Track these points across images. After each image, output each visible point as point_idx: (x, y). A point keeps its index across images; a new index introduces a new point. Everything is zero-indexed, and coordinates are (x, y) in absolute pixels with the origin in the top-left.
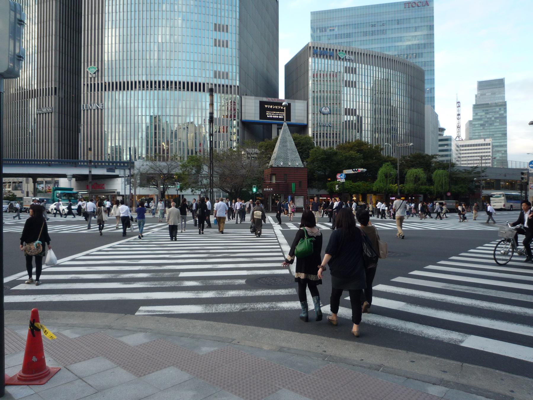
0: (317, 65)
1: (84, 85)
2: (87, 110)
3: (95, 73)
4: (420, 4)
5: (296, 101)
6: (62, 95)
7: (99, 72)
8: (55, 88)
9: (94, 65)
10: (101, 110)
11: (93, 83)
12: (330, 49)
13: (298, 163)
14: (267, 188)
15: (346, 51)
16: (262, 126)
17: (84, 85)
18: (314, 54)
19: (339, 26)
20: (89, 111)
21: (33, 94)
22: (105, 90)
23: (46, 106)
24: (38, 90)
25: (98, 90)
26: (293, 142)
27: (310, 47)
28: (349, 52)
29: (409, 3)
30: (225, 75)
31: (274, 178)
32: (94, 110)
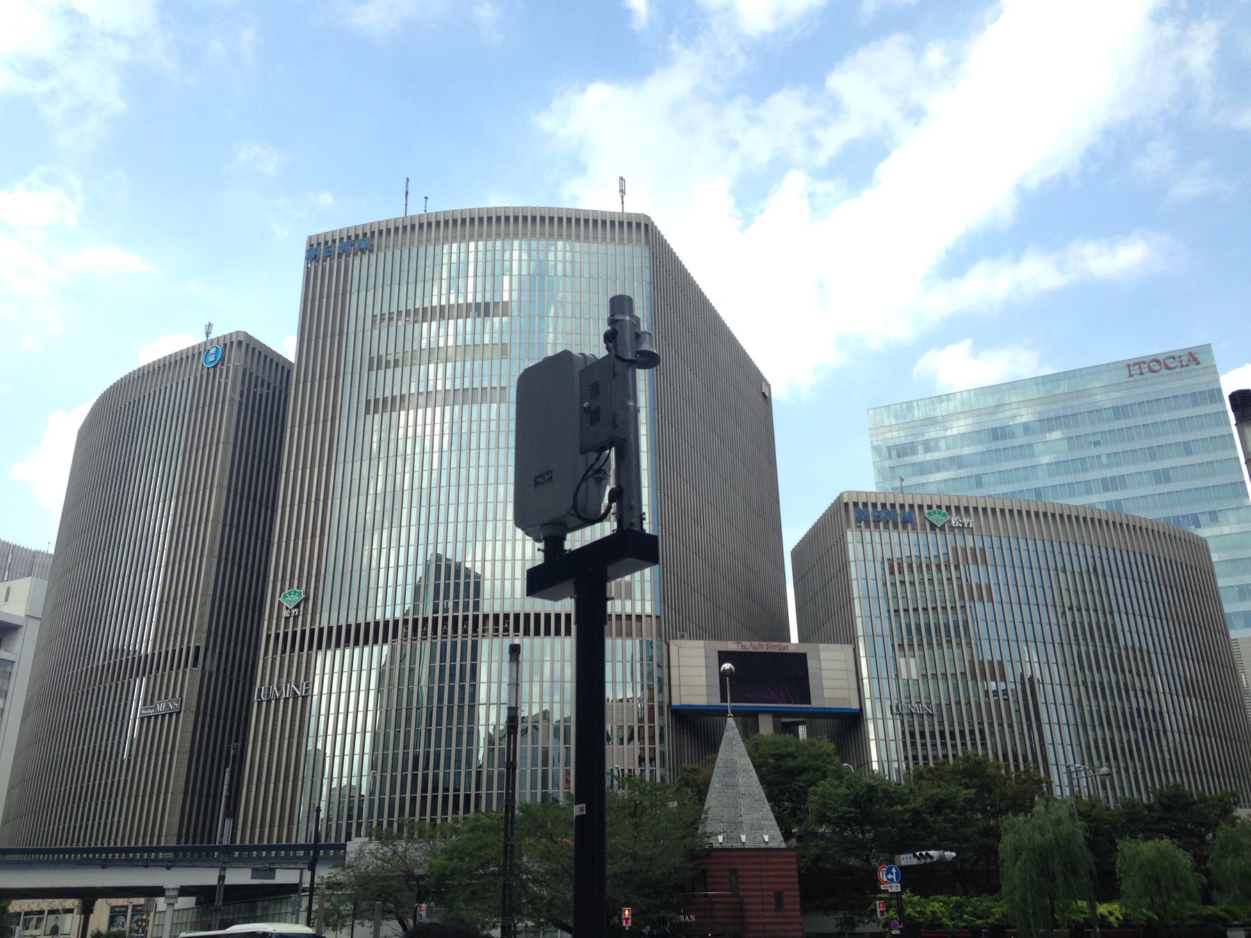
0: (869, 547)
1: (269, 636)
2: (269, 702)
3: (298, 606)
4: (1171, 363)
5: (821, 646)
6: (211, 665)
8: (197, 648)
10: (305, 698)
13: (771, 836)
15: (948, 508)
17: (269, 636)
18: (858, 520)
21: (141, 666)
22: (319, 648)
23: (174, 695)
24: (153, 654)
25: (301, 649)
26: (754, 774)
27: (846, 505)
28: (957, 508)
29: (1139, 363)
32: (286, 700)
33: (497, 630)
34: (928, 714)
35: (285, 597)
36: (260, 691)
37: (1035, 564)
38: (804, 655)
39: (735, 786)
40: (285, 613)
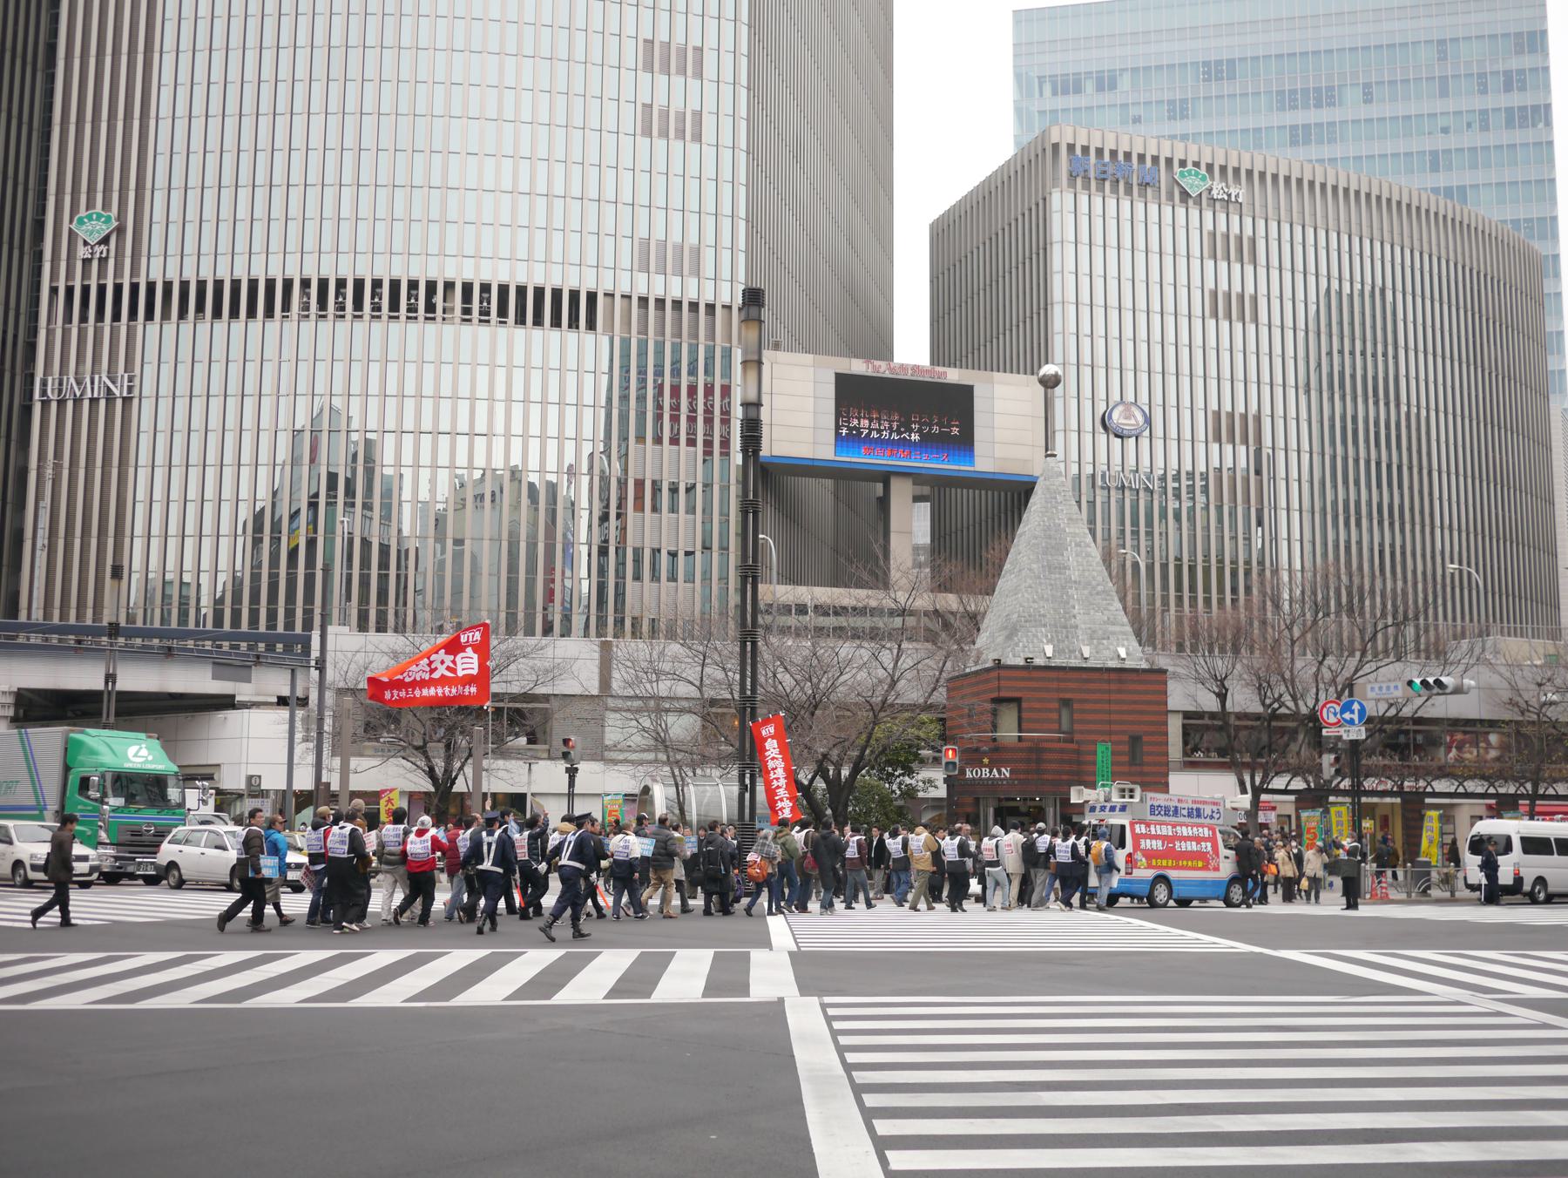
2: (61, 403)
3: (105, 241)
7: (126, 235)
9: (106, 205)
10: (127, 401)
11: (93, 284)
12: (1142, 158)
14: (982, 765)
15: (1210, 167)
16: (829, 483)
18: (1072, 177)
19: (1135, 70)
20: (70, 404)
22: (149, 315)
27: (1056, 147)
28: (1223, 169)
30: (689, 261)
31: (1008, 718)
33: (467, 311)
34: (1147, 489)
35: (81, 222)
36: (44, 383)
37: (1127, 303)
38: (971, 387)
39: (1063, 568)
40: (82, 252)
